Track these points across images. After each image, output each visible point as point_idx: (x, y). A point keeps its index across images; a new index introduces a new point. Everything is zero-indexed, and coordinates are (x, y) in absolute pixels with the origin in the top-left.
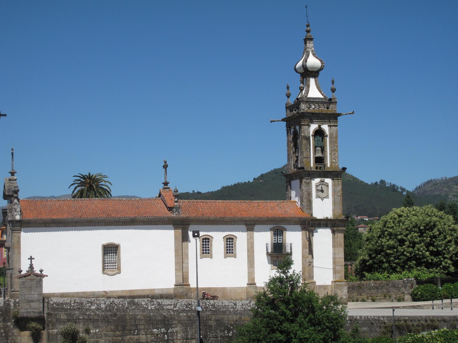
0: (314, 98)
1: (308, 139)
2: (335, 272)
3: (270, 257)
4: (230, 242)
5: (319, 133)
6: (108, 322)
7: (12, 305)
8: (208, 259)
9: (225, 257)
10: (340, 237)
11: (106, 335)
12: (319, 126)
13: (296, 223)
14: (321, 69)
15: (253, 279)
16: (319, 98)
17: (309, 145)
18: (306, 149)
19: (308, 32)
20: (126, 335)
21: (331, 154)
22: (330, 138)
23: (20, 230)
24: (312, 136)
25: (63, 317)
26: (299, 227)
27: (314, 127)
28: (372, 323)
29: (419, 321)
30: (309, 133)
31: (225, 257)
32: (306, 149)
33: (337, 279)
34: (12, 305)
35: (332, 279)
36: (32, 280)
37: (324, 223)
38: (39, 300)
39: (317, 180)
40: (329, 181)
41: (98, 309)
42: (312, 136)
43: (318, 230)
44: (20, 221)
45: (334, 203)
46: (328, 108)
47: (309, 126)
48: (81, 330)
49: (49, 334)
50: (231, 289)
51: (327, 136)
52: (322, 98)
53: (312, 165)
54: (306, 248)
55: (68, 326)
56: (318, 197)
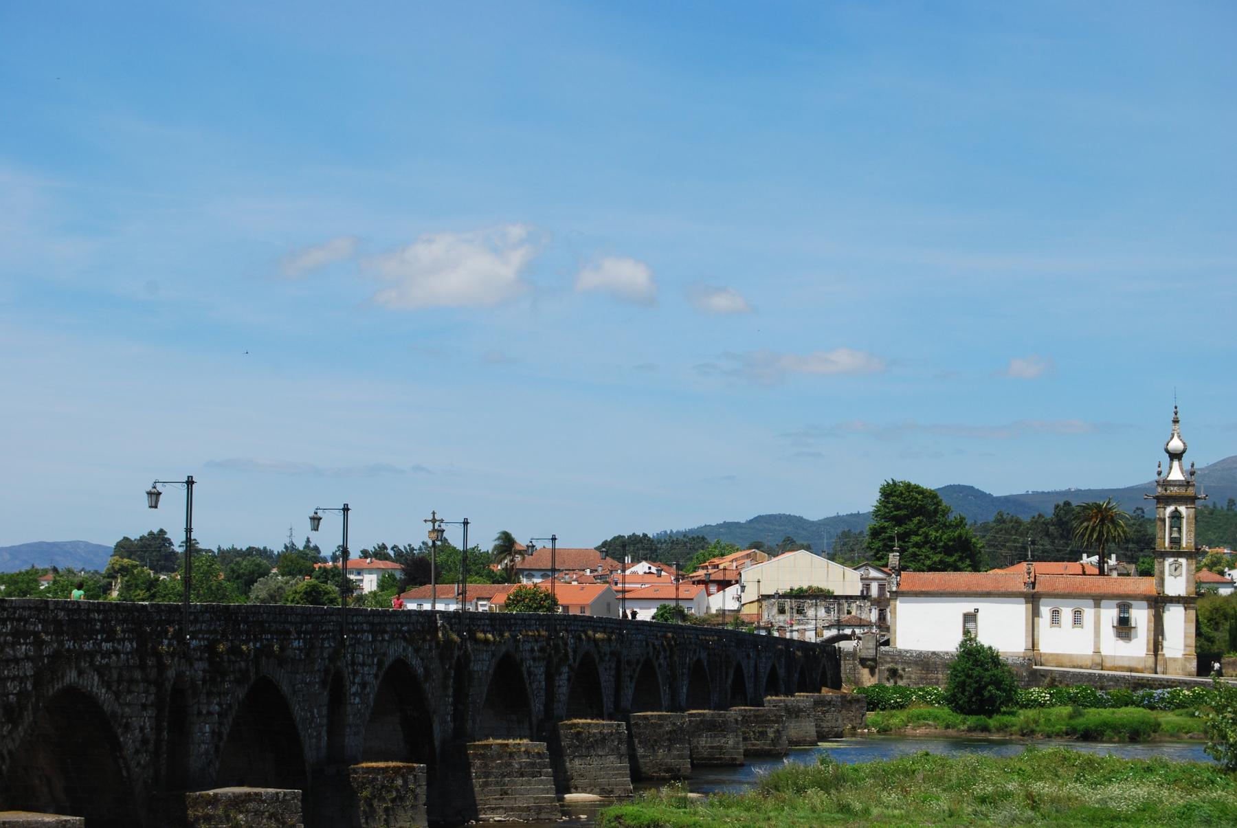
0: (1173, 481)
1: (1164, 520)
2: (1186, 646)
3: (1115, 630)
4: (1078, 614)
5: (1176, 516)
6: (917, 665)
7: (858, 650)
8: (1058, 628)
9: (1073, 628)
10: (1192, 613)
11: (916, 673)
12: (1176, 508)
13: (1142, 599)
14: (1184, 451)
15: (1099, 648)
16: (1179, 481)
17: (1163, 526)
18: (1161, 530)
19: (1176, 414)
20: (929, 674)
21: (1187, 534)
22: (1187, 519)
23: (896, 599)
24: (1169, 517)
25: (889, 659)
26: (1023, 600)
27: (1170, 509)
28: (1118, 680)
29: (1161, 681)
30: (1164, 515)
31: (1073, 628)
32: (1161, 530)
33: (1187, 653)
34: (858, 650)
35: (1182, 652)
36: (869, 636)
37: (1177, 600)
38: (873, 648)
39: (1171, 560)
40: (1183, 561)
41: (911, 656)
42: (1169, 517)
43: (1171, 608)
44: (896, 592)
45: (1188, 581)
46: (1186, 491)
47: (1165, 508)
48: (899, 668)
49: (879, 669)
50: (1077, 656)
51: (1183, 518)
52: (1182, 481)
53: (1167, 545)
54: (1151, 622)
55: (890, 665)
56: (1171, 575)
